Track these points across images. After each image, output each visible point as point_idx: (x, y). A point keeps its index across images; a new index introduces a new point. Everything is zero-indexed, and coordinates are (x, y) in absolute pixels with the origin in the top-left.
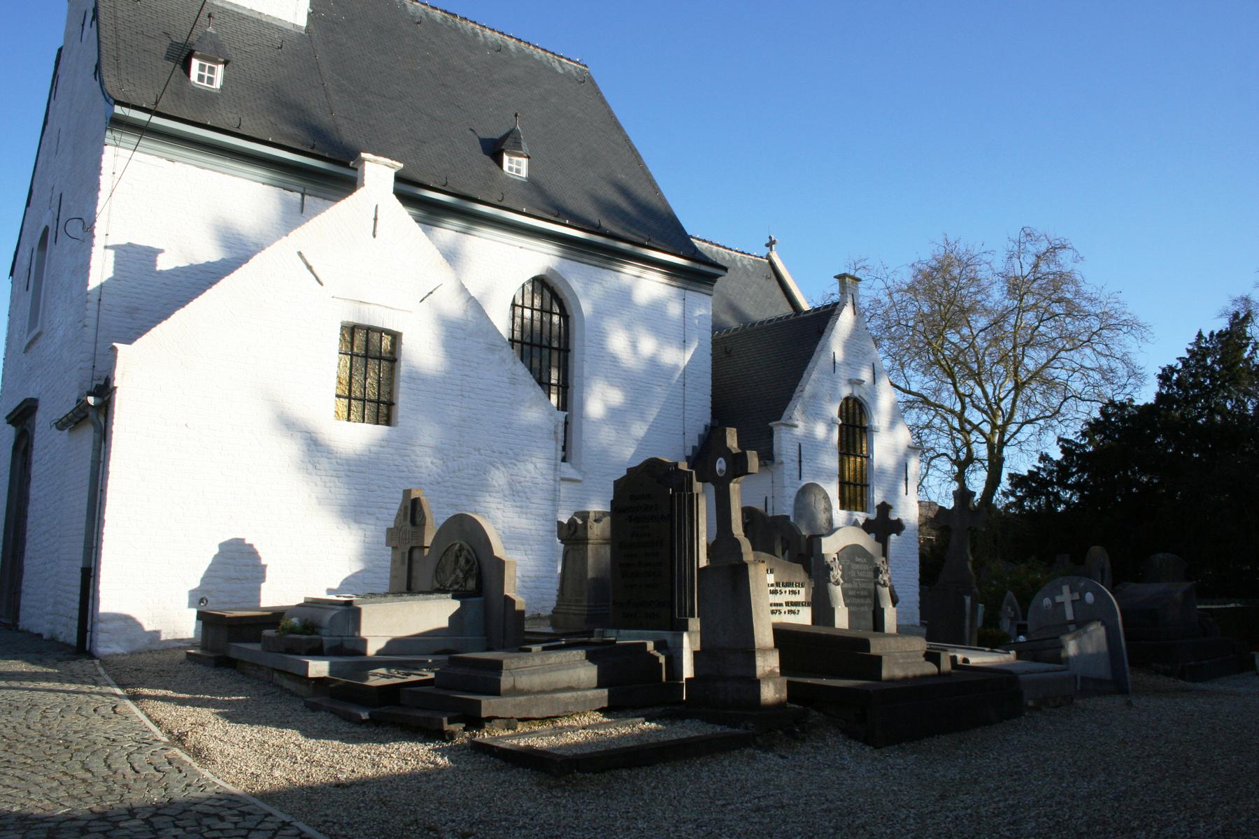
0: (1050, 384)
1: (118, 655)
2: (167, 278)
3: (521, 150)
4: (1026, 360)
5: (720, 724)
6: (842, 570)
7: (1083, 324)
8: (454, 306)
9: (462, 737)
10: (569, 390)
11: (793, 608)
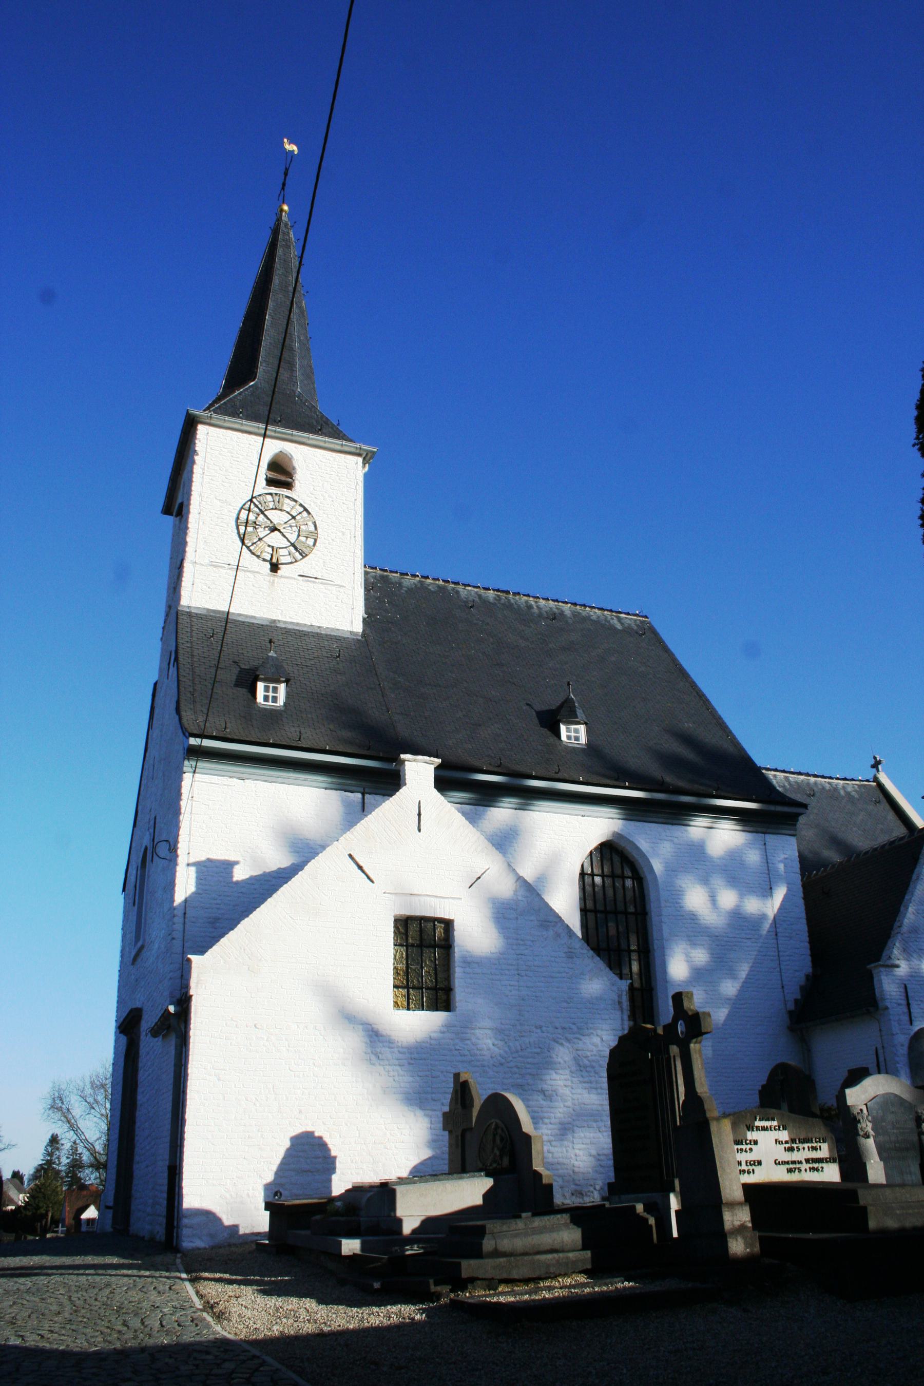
2: (244, 887)
3: (577, 718)
8: (505, 888)
11: (816, 1165)
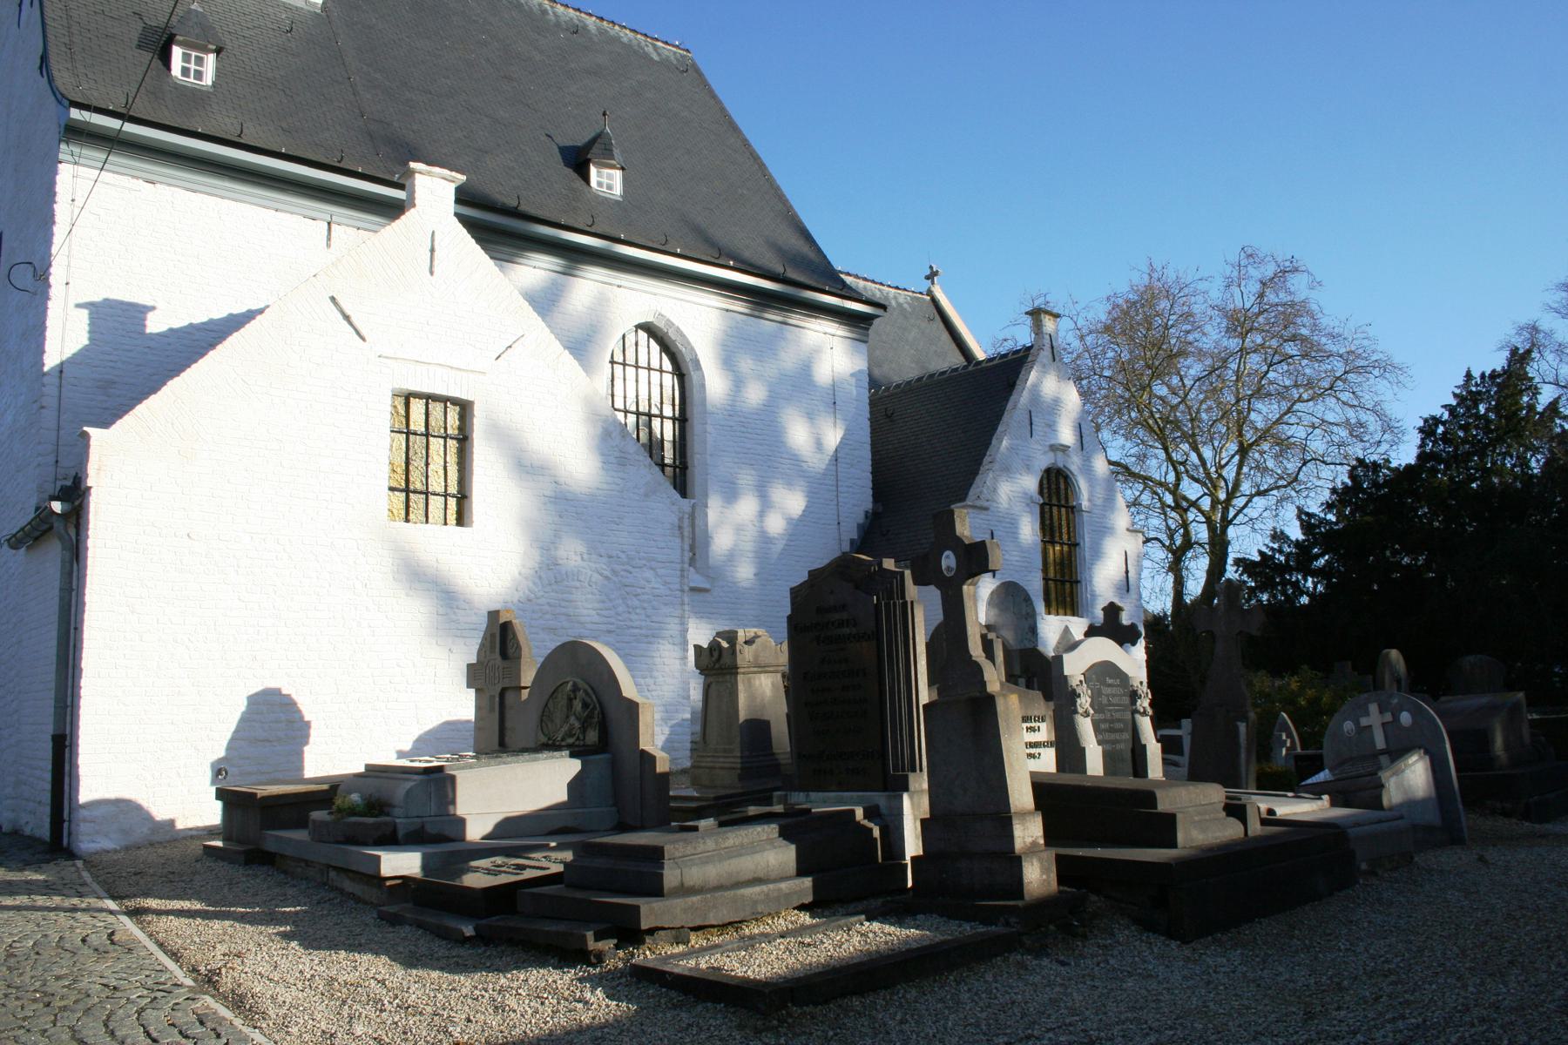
0: (1284, 445)
1: (108, 852)
3: (614, 159)
4: (1253, 416)
5: (968, 920)
6: (1092, 697)
7: (1324, 367)
9: (616, 959)
10: (688, 472)
11: (1032, 751)
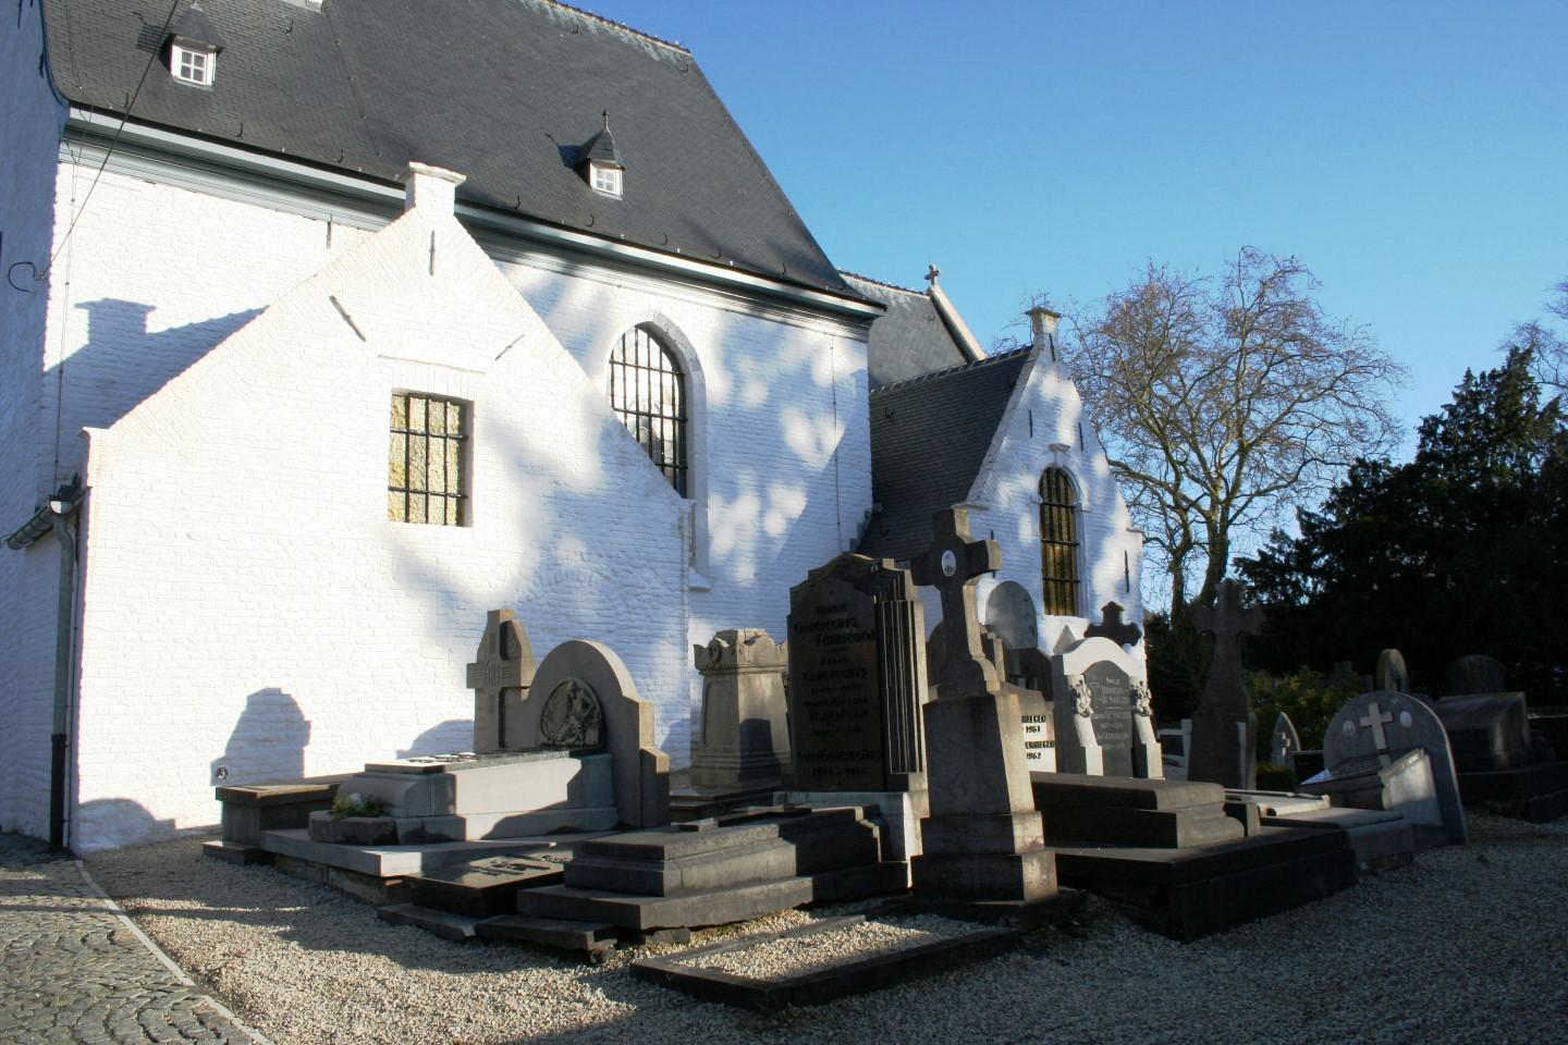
0: (1284, 445)
3: (613, 159)
4: (1253, 416)
6: (1092, 697)
9: (616, 958)
11: (1033, 751)
